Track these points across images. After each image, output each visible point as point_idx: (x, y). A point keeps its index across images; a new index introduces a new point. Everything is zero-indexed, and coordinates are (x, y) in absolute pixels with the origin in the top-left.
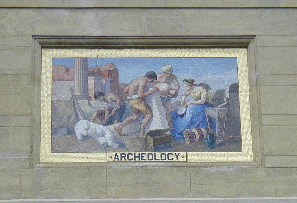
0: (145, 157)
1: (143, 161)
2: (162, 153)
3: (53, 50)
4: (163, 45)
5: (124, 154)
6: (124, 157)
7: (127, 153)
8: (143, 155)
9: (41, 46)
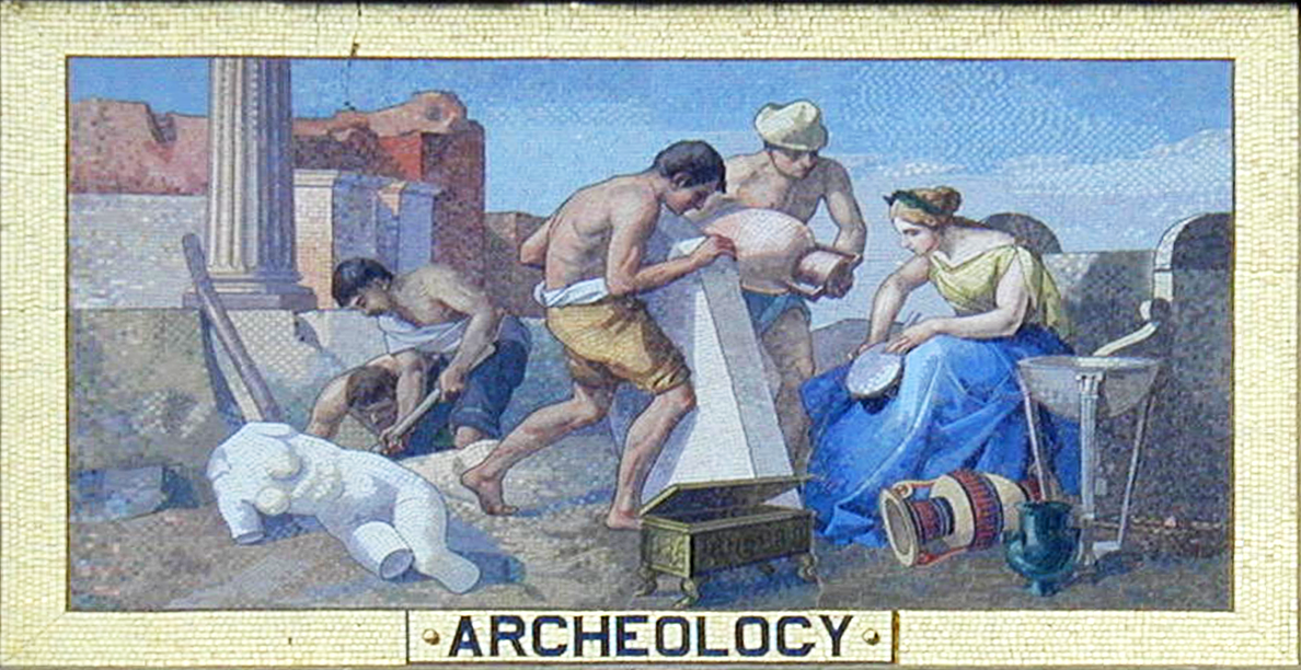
5: (510, 620)
6: (514, 638)
8: (629, 628)
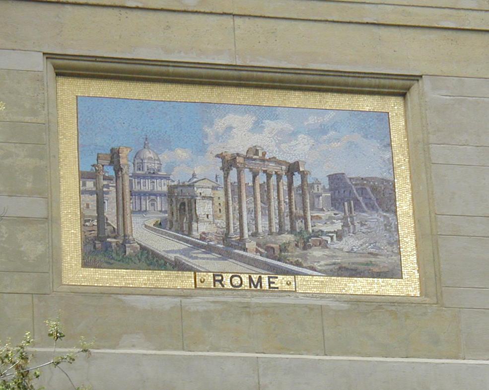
3: (85, 82)
4: (125, 73)
8: (271, 280)
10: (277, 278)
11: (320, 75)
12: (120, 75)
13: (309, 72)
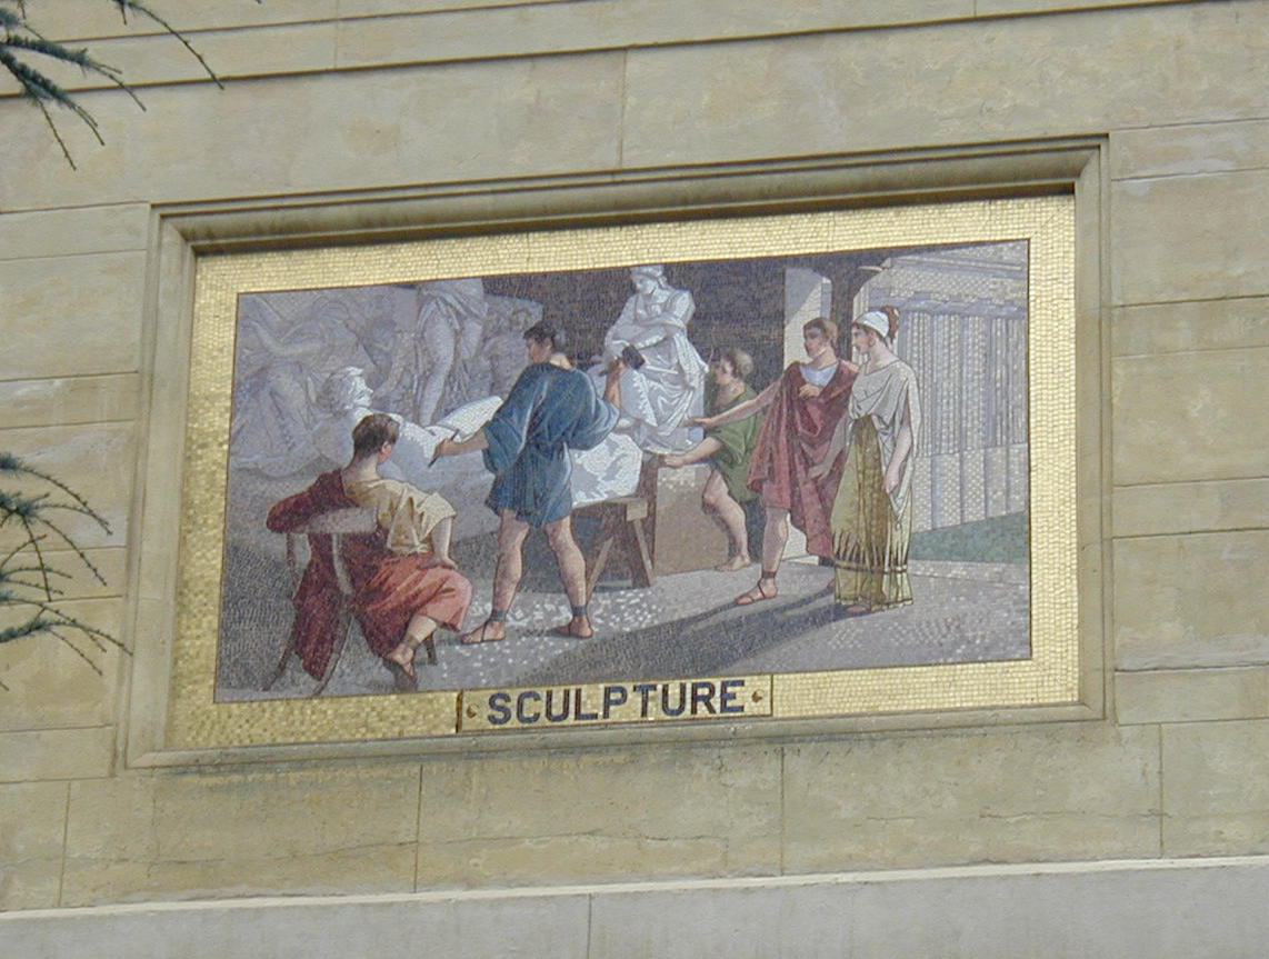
0: (738, 698)
1: (582, 722)
2: (699, 681)
4: (745, 200)
5: (704, 685)
6: (706, 700)
7: (717, 683)
8: (730, 690)
9: (193, 247)
10: (742, 683)
11: (493, 192)
12: (641, 211)
13: (287, 202)
